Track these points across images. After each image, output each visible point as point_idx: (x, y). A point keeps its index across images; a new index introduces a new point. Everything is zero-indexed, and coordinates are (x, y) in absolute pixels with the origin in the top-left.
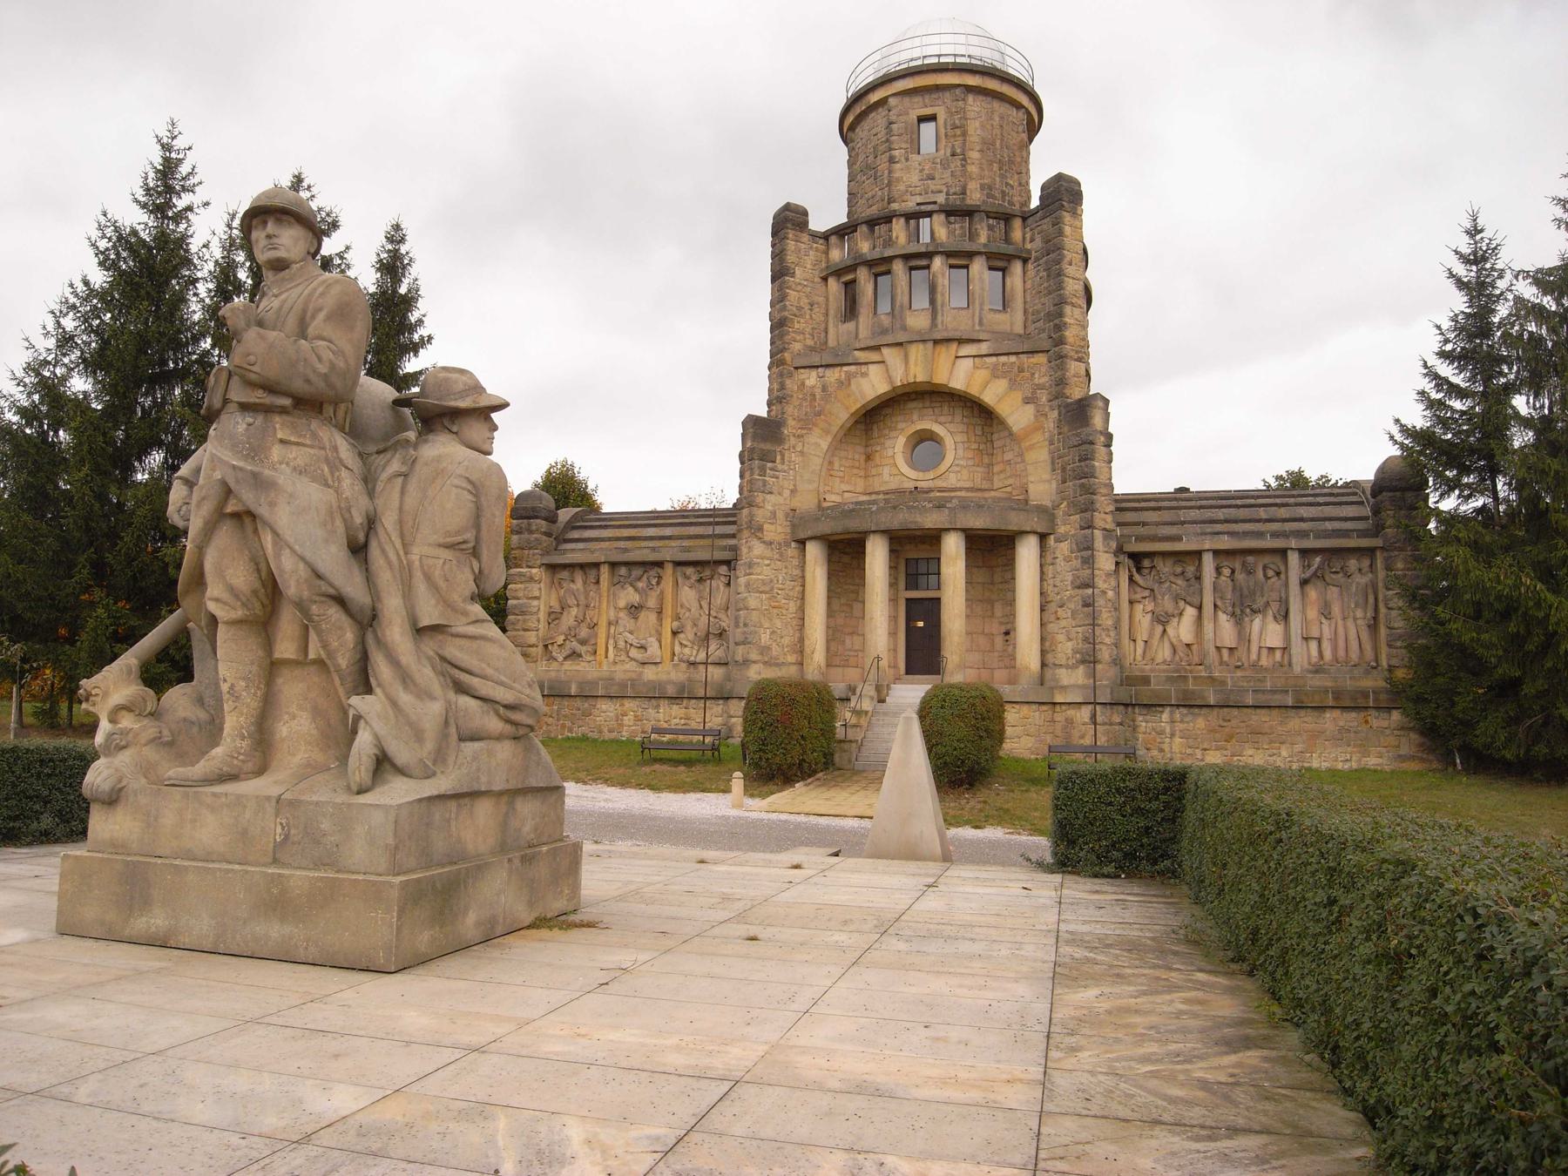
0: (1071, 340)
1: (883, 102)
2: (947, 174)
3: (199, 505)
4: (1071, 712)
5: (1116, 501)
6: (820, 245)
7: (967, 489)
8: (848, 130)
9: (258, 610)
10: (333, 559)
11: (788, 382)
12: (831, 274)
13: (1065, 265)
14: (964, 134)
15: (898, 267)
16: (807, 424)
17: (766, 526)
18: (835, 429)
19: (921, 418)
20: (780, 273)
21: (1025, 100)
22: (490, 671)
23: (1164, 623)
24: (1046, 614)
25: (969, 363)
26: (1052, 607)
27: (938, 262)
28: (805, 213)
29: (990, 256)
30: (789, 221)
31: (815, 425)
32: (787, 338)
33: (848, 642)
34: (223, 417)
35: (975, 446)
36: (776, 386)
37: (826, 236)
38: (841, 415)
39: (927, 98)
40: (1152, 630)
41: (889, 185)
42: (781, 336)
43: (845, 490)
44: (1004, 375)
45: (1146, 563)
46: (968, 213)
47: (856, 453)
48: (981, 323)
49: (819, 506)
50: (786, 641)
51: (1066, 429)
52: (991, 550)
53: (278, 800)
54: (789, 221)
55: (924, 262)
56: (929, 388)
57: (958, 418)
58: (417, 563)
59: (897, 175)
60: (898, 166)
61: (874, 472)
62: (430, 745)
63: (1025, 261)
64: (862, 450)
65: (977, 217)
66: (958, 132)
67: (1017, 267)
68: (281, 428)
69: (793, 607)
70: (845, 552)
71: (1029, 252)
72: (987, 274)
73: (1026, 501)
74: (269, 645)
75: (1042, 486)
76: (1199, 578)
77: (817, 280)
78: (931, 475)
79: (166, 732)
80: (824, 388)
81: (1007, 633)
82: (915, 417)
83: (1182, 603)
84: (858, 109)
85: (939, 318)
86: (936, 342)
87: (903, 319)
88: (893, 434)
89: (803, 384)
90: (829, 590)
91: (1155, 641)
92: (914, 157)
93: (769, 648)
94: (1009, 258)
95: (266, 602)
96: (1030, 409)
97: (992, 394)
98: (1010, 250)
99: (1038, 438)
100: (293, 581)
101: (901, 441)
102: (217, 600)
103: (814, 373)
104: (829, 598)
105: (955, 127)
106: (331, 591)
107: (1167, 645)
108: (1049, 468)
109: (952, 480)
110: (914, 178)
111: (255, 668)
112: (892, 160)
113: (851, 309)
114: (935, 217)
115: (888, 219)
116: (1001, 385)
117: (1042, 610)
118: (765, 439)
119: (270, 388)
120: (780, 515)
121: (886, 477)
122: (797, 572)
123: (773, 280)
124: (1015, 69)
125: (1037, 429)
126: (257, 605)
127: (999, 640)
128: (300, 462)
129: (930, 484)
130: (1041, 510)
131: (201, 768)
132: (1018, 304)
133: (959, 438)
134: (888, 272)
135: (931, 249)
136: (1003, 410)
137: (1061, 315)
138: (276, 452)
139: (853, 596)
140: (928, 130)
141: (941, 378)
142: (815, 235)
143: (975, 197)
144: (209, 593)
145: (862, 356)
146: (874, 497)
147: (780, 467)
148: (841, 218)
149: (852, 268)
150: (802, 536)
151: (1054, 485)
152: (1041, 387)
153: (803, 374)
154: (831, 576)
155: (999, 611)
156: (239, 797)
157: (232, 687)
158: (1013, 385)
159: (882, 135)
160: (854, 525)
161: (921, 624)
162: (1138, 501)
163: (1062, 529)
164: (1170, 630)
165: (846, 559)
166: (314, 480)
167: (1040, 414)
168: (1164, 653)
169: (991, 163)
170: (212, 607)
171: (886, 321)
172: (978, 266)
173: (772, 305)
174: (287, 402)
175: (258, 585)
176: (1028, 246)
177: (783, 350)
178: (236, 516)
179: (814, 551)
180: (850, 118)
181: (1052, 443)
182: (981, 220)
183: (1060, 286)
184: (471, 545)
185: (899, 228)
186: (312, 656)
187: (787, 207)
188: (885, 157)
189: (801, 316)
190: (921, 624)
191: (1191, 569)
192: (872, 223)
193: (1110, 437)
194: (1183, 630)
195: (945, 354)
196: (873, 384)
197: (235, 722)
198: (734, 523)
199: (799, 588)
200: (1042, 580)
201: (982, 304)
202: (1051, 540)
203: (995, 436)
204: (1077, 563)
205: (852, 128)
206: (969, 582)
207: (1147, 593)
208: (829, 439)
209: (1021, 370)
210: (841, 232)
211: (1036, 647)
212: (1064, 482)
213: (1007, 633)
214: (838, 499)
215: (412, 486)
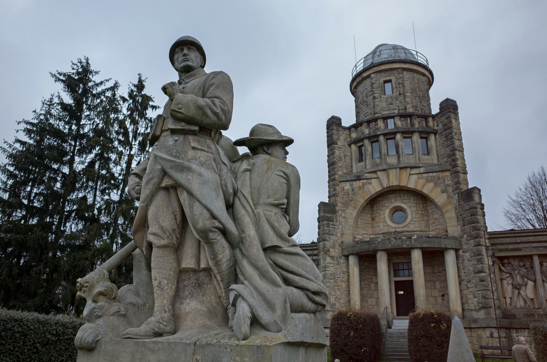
0: (460, 165)
1: (369, 76)
2: (398, 102)
3: (147, 183)
4: (480, 332)
5: (490, 235)
6: (347, 132)
7: (420, 231)
8: (354, 89)
9: (175, 241)
10: (219, 206)
11: (337, 187)
12: (352, 143)
13: (454, 134)
14: (404, 86)
15: (382, 138)
16: (346, 205)
17: (331, 249)
18: (359, 207)
19: (395, 201)
20: (331, 143)
21: (427, 73)
22: (303, 273)
23: (519, 289)
24: (462, 286)
25: (416, 176)
26: (464, 283)
27: (398, 136)
28: (340, 119)
29: (420, 132)
30: (334, 123)
31: (350, 205)
32: (336, 170)
33: (369, 301)
34: (161, 139)
35: (420, 212)
36: (332, 190)
37: (349, 128)
38: (361, 201)
39: (387, 73)
40: (513, 293)
41: (374, 107)
42: (333, 169)
43: (365, 234)
44: (432, 181)
45: (506, 261)
46: (410, 116)
47: (367, 217)
48: (419, 160)
49: (354, 241)
50: (342, 301)
51: (462, 203)
52: (434, 257)
53: (195, 343)
54: (334, 123)
55: (392, 136)
56: (399, 188)
57: (412, 201)
58: (262, 213)
59: (377, 103)
60: (377, 100)
61: (376, 225)
62: (279, 312)
63: (435, 134)
64: (370, 216)
65: (413, 118)
66: (401, 86)
67: (432, 137)
68: (193, 141)
69: (344, 285)
70: (367, 260)
71: (437, 130)
72: (419, 140)
73: (447, 236)
74: (179, 261)
75: (454, 229)
76: (532, 268)
77: (347, 146)
78: (402, 225)
79: (122, 309)
80: (353, 190)
81: (443, 296)
82: (393, 201)
83: (526, 279)
84: (358, 80)
85: (401, 159)
86: (401, 168)
87: (385, 160)
88: (384, 208)
89: (343, 188)
90: (360, 278)
91: (515, 298)
92: (383, 96)
93: (335, 304)
94: (429, 133)
95: (179, 236)
96: (445, 195)
97: (426, 190)
98: (429, 130)
99: (449, 207)
100: (199, 218)
101: (387, 211)
102: (154, 234)
103: (348, 184)
104: (360, 281)
105: (399, 84)
106: (220, 226)
107: (521, 299)
108: (456, 220)
109: (411, 228)
110: (384, 104)
111: (172, 273)
112: (374, 98)
113: (361, 159)
114: (396, 118)
115: (376, 120)
116: (431, 185)
117: (460, 284)
118: (328, 212)
119: (189, 121)
120: (337, 244)
121: (382, 227)
122: (345, 269)
123: (328, 146)
124: (421, 60)
125: (449, 203)
126: (175, 239)
127: (440, 299)
128: (202, 159)
129: (402, 229)
130: (454, 238)
131: (144, 328)
132: (434, 151)
133: (413, 209)
134: (377, 141)
135: (395, 131)
136: (432, 196)
137: (454, 155)
138: (191, 153)
139: (370, 280)
140: (388, 86)
141: (404, 183)
142: (345, 128)
143: (410, 110)
144: (150, 230)
145: (368, 175)
146: (377, 236)
147: (336, 223)
148: (354, 121)
149: (362, 140)
150: (346, 253)
151: (459, 227)
152: (448, 185)
153: (343, 184)
154: (361, 271)
155: (438, 285)
156: (169, 343)
157: (160, 283)
158: (436, 185)
159: (369, 89)
160: (372, 247)
161: (402, 293)
162: (495, 234)
163: (465, 247)
164: (522, 293)
165: (366, 264)
166: (208, 169)
167: (449, 197)
168: (521, 303)
169: (415, 97)
170: (151, 238)
171: (378, 161)
172: (416, 137)
173: (328, 156)
174: (196, 128)
175: (175, 227)
176: (436, 128)
177: (335, 174)
178: (166, 189)
179: (352, 260)
180: (355, 83)
181: (456, 209)
182: (415, 119)
183: (453, 143)
184: (285, 206)
185: (380, 123)
186: (203, 266)
187: (333, 117)
188: (371, 97)
189: (341, 160)
190: (402, 293)
191: (528, 264)
192: (369, 122)
193: (483, 205)
194: (529, 291)
195: (405, 174)
196: (374, 187)
197: (161, 301)
198: (316, 249)
199: (346, 277)
200: (459, 270)
201: (419, 152)
202: (461, 252)
203: (429, 208)
204: (475, 262)
205: (356, 87)
206: (425, 273)
207: (508, 275)
208: (356, 211)
209: (439, 179)
210: (355, 126)
211: (459, 302)
212: (464, 226)
213: (443, 296)
214: (361, 237)
215: (255, 176)
